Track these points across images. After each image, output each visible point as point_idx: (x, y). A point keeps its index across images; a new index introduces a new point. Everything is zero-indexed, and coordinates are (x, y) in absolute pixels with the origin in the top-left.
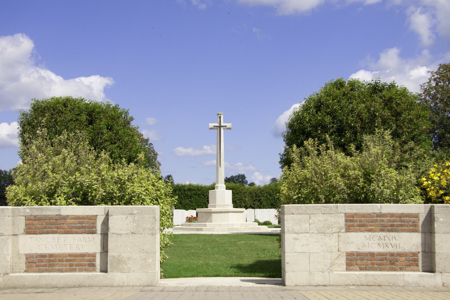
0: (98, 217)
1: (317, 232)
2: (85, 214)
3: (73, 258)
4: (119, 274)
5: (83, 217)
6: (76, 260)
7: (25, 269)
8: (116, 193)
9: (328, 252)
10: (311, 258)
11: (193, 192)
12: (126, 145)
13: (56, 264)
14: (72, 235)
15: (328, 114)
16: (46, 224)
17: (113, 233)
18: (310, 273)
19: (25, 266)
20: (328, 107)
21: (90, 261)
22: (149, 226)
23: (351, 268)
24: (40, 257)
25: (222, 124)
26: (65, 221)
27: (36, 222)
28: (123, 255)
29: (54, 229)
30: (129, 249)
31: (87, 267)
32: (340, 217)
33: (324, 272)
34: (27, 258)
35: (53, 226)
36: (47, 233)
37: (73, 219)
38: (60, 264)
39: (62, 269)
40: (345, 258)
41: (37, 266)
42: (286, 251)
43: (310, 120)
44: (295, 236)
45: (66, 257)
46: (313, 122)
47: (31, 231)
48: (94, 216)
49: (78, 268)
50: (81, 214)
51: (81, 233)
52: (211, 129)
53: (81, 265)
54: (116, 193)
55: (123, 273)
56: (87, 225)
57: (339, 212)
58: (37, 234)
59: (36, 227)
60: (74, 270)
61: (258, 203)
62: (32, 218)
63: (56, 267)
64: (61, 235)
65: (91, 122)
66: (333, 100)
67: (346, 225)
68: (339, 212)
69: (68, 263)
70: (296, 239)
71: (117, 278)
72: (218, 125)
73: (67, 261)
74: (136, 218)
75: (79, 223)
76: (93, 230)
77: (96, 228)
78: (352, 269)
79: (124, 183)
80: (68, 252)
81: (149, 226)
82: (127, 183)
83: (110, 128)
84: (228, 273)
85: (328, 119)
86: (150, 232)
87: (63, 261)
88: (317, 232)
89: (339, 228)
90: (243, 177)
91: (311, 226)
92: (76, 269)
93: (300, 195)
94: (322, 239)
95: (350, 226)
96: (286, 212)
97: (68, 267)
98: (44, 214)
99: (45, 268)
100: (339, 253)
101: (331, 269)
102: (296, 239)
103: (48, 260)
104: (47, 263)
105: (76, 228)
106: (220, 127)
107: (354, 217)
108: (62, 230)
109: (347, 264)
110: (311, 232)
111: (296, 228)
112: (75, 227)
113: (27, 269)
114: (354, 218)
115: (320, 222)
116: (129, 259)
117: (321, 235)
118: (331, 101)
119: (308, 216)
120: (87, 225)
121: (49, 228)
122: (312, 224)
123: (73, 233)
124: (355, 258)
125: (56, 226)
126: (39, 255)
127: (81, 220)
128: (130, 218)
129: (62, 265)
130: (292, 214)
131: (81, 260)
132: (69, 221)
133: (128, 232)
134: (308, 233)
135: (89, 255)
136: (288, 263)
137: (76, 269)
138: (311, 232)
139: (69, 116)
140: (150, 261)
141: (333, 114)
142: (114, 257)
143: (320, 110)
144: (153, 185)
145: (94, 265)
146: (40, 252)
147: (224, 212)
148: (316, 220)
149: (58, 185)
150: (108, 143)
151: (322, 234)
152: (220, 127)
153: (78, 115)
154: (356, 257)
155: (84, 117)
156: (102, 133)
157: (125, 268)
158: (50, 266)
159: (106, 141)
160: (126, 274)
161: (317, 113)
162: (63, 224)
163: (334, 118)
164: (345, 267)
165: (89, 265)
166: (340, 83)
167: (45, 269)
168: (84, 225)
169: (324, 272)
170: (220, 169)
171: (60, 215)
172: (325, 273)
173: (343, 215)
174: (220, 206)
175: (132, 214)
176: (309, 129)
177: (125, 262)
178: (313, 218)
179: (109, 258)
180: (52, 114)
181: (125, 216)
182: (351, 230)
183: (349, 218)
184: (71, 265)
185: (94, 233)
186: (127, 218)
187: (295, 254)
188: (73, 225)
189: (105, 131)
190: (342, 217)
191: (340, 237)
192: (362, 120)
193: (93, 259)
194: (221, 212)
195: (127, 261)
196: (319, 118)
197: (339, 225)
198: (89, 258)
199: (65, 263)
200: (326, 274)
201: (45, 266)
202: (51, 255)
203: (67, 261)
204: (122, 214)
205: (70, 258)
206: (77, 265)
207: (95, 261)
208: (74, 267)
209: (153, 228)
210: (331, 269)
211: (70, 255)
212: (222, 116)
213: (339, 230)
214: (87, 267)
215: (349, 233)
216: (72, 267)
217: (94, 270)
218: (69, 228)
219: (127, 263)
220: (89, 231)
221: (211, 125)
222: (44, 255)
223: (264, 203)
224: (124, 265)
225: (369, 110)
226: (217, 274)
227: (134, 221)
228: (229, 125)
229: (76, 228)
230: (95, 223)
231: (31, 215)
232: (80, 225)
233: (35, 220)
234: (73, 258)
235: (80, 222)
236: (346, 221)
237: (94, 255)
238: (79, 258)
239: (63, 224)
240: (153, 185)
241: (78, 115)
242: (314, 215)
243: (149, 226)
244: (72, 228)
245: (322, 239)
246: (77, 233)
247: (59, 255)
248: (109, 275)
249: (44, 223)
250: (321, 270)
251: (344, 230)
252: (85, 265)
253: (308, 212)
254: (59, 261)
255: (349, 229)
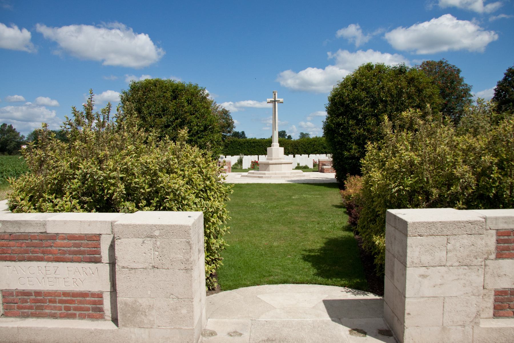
0: (102, 237)
1: (457, 264)
2: (82, 233)
3: (69, 298)
4: (136, 330)
5: (79, 236)
6: (74, 301)
7: (2, 312)
8: (144, 188)
9: (473, 295)
10: (446, 305)
11: (256, 144)
12: (202, 115)
13: (47, 306)
14: (65, 263)
15: (363, 90)
16: (27, 247)
17: (123, 267)
18: (444, 329)
19: (2, 307)
20: (362, 84)
21: (94, 303)
22: (180, 256)
23: (501, 312)
24: (22, 295)
25: (277, 99)
26: (54, 243)
27: (12, 243)
28: (140, 301)
29: (40, 255)
30: (149, 292)
31: (91, 312)
32: (489, 237)
33: (464, 326)
34: (3, 296)
35: (37, 249)
36: (30, 259)
37: (65, 239)
38: (51, 306)
39: (55, 313)
40: (492, 298)
41: (19, 308)
42: (407, 296)
43: (348, 95)
44: (422, 271)
45: (60, 296)
46: (351, 97)
47: (6, 257)
48: (95, 235)
49: (78, 313)
50: (77, 233)
51: (80, 261)
52: (268, 103)
53: (81, 309)
54: (144, 188)
55: (143, 330)
56: (86, 249)
57: (488, 228)
58: (15, 261)
59: (13, 250)
60: (72, 316)
61: (296, 150)
62: (6, 237)
63: (47, 311)
64: (50, 263)
65: (175, 98)
66: (366, 79)
67: (497, 248)
68: (488, 228)
69: (63, 305)
70: (424, 276)
71: (133, 336)
72: (273, 100)
73: (61, 302)
74: (158, 243)
75: (75, 245)
76: (95, 258)
77: (100, 254)
78: (502, 315)
79: (155, 174)
80: (62, 289)
81: (179, 256)
82: (160, 174)
83: (189, 102)
84: (298, 277)
85: (363, 94)
86: (183, 267)
87: (55, 302)
88: (457, 264)
89: (487, 253)
90: (284, 132)
91: (449, 255)
92: (75, 314)
93: (401, 187)
94: (465, 274)
95: (503, 249)
96: (409, 233)
97: (63, 311)
98: (22, 230)
99: (30, 311)
100: (485, 291)
101: (477, 320)
102: (424, 276)
103: (33, 299)
104: (33, 304)
105: (71, 253)
106: (275, 101)
107: (510, 236)
108: (50, 256)
109: (495, 308)
110: (448, 264)
111: (426, 259)
112: (69, 251)
113: (5, 313)
114: (510, 237)
115: (464, 247)
116: (151, 307)
117: (464, 269)
118: (364, 80)
119: (445, 238)
120: (86, 249)
121: (33, 252)
122: (450, 251)
123: (66, 262)
124: (508, 298)
125: (42, 249)
126: (21, 292)
127: (77, 241)
128: (149, 243)
129: (55, 308)
130: (420, 236)
131: (80, 302)
132: (58, 241)
133: (146, 265)
134: (444, 266)
135: (93, 295)
136: (409, 314)
137: (75, 314)
138: (448, 264)
139: (158, 93)
140: (184, 311)
141: (367, 90)
142: (126, 304)
143: (356, 87)
144: (201, 172)
145: (101, 310)
146: (21, 287)
147: (279, 164)
148: (458, 245)
149: (64, 178)
150: (188, 114)
151: (466, 267)
152: (275, 101)
153: (165, 92)
154: (509, 296)
155: (168, 94)
156: (183, 106)
157: (146, 321)
158: (38, 308)
159: (186, 112)
160: (147, 330)
161: (353, 89)
162: (51, 246)
163: (367, 93)
164: (491, 312)
165: (94, 310)
166: (370, 67)
167: (32, 313)
168: (82, 249)
169: (464, 326)
170: (275, 132)
171: (45, 232)
172: (467, 328)
173: (494, 232)
174: (275, 159)
175: (151, 237)
176: (347, 102)
177: (145, 312)
178: (452, 242)
179: (118, 306)
180: (144, 92)
181: (141, 240)
182: (504, 256)
183: (502, 238)
184: (67, 309)
185: (98, 261)
186: (143, 242)
187: (422, 300)
188: (65, 249)
189: (186, 104)
190: (492, 237)
191: (487, 267)
192: (391, 94)
193: (99, 301)
194: (276, 164)
195: (147, 311)
196: (356, 93)
197: (487, 249)
198: (93, 299)
199: (58, 305)
200: (468, 329)
201: (31, 308)
202: (38, 293)
203: (61, 302)
204: (135, 236)
205: (64, 298)
206: (76, 309)
207: (102, 304)
208: (72, 312)
209: (187, 260)
210: (477, 320)
211: (65, 294)
212: (276, 93)
213: (486, 256)
214: (91, 312)
215: (500, 261)
216: (69, 312)
217: (102, 317)
218: (61, 253)
219: (147, 314)
220: (90, 258)
221: (269, 100)
222: (28, 292)
223: (300, 150)
224: (143, 317)
225: (396, 87)
226: (285, 278)
227: (155, 248)
228: (281, 100)
229: (71, 253)
230: (98, 246)
231: (5, 232)
232: (75, 248)
233: (10, 240)
234: (69, 298)
235: (75, 244)
236: (498, 241)
237: (100, 295)
238: (78, 298)
239: (51, 246)
240: (201, 172)
241: (165, 92)
242: (455, 237)
243: (179, 256)
244: (64, 252)
245: (465, 274)
246: (72, 261)
247: (49, 293)
248: (123, 330)
249: (23, 245)
250: (461, 323)
251: (493, 256)
252: (88, 309)
253: (445, 232)
254: (50, 301)
255: (502, 255)
